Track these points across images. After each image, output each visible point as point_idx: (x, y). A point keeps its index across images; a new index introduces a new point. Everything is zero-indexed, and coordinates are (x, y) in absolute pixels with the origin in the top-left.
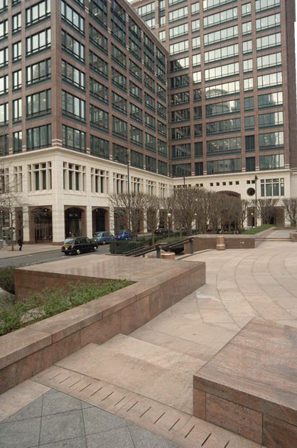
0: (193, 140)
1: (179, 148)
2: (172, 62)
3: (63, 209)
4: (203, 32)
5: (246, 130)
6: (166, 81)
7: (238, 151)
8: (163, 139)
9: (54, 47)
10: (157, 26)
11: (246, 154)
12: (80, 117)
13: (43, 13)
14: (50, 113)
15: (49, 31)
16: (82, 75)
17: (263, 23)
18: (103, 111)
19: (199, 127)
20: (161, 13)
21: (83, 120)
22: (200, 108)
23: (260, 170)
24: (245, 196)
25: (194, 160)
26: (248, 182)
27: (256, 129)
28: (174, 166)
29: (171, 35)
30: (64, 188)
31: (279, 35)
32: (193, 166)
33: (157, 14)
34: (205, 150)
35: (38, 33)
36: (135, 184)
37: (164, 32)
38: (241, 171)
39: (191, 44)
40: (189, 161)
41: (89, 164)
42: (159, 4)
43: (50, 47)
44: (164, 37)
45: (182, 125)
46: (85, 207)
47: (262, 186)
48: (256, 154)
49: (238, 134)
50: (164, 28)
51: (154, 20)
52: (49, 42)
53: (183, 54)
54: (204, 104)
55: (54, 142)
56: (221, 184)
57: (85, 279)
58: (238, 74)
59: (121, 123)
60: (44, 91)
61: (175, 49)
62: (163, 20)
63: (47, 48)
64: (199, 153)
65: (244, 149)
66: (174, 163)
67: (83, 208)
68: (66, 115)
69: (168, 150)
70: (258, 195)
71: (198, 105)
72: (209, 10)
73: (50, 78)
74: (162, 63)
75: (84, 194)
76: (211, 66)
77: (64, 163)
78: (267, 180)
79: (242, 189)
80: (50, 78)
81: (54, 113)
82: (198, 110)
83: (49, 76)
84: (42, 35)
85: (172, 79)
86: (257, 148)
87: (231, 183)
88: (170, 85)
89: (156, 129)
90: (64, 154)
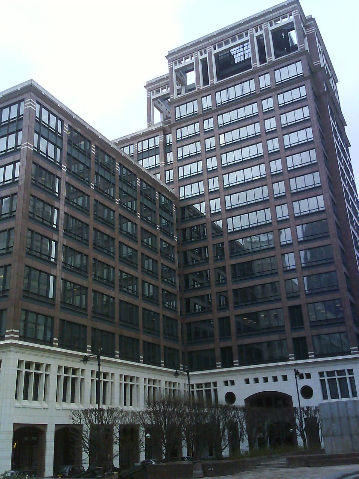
0: (216, 315)
1: (196, 301)
2: (183, 209)
3: (12, 429)
4: (221, 172)
5: (288, 298)
6: (175, 233)
7: (280, 330)
8: (171, 290)
9: (22, 182)
10: (163, 164)
11: (290, 335)
12: (55, 159)
13: (14, 114)
14: (7, 296)
15: (20, 133)
16: (60, 122)
17: (296, 160)
18: (82, 254)
19: (224, 321)
20: (167, 148)
21: (53, 260)
22: (224, 268)
23: (316, 357)
24: (299, 402)
25: (217, 345)
26: (226, 383)
27: (303, 296)
28: (190, 353)
29: (181, 174)
30: (16, 398)
31: (310, 130)
32: (218, 353)
33: (162, 150)
34: (233, 329)
35: (9, 106)
36: (126, 385)
37: (171, 171)
38: (288, 360)
39: (207, 185)
40: (211, 346)
41: (55, 361)
42: (165, 139)
43: (17, 182)
44: (172, 177)
45: (200, 293)
46: (45, 425)
47: (323, 382)
48: (306, 332)
49: (279, 305)
50: (170, 167)
51: (158, 156)
52: (16, 176)
53: (199, 197)
54: (225, 240)
55: (8, 333)
56: (261, 380)
57: (48, 104)
58: (270, 223)
59: (106, 211)
60: (6, 230)
61: (188, 191)
62: (170, 157)
63: (14, 181)
64: (225, 334)
65: (288, 327)
66: (190, 349)
67: (42, 428)
68: (31, 255)
69: (178, 305)
70: (317, 400)
71: (218, 240)
72: (226, 146)
73: (10, 253)
74: (167, 211)
75: (45, 405)
76: (232, 191)
77: (20, 362)
78: (330, 373)
79: (289, 387)
80: (10, 253)
81: (19, 215)
82: (219, 250)
83: (10, 250)
84: (10, 168)
85: (184, 230)
86: (307, 324)
87: (275, 379)
88: (181, 238)
89: (160, 276)
90: (21, 350)
